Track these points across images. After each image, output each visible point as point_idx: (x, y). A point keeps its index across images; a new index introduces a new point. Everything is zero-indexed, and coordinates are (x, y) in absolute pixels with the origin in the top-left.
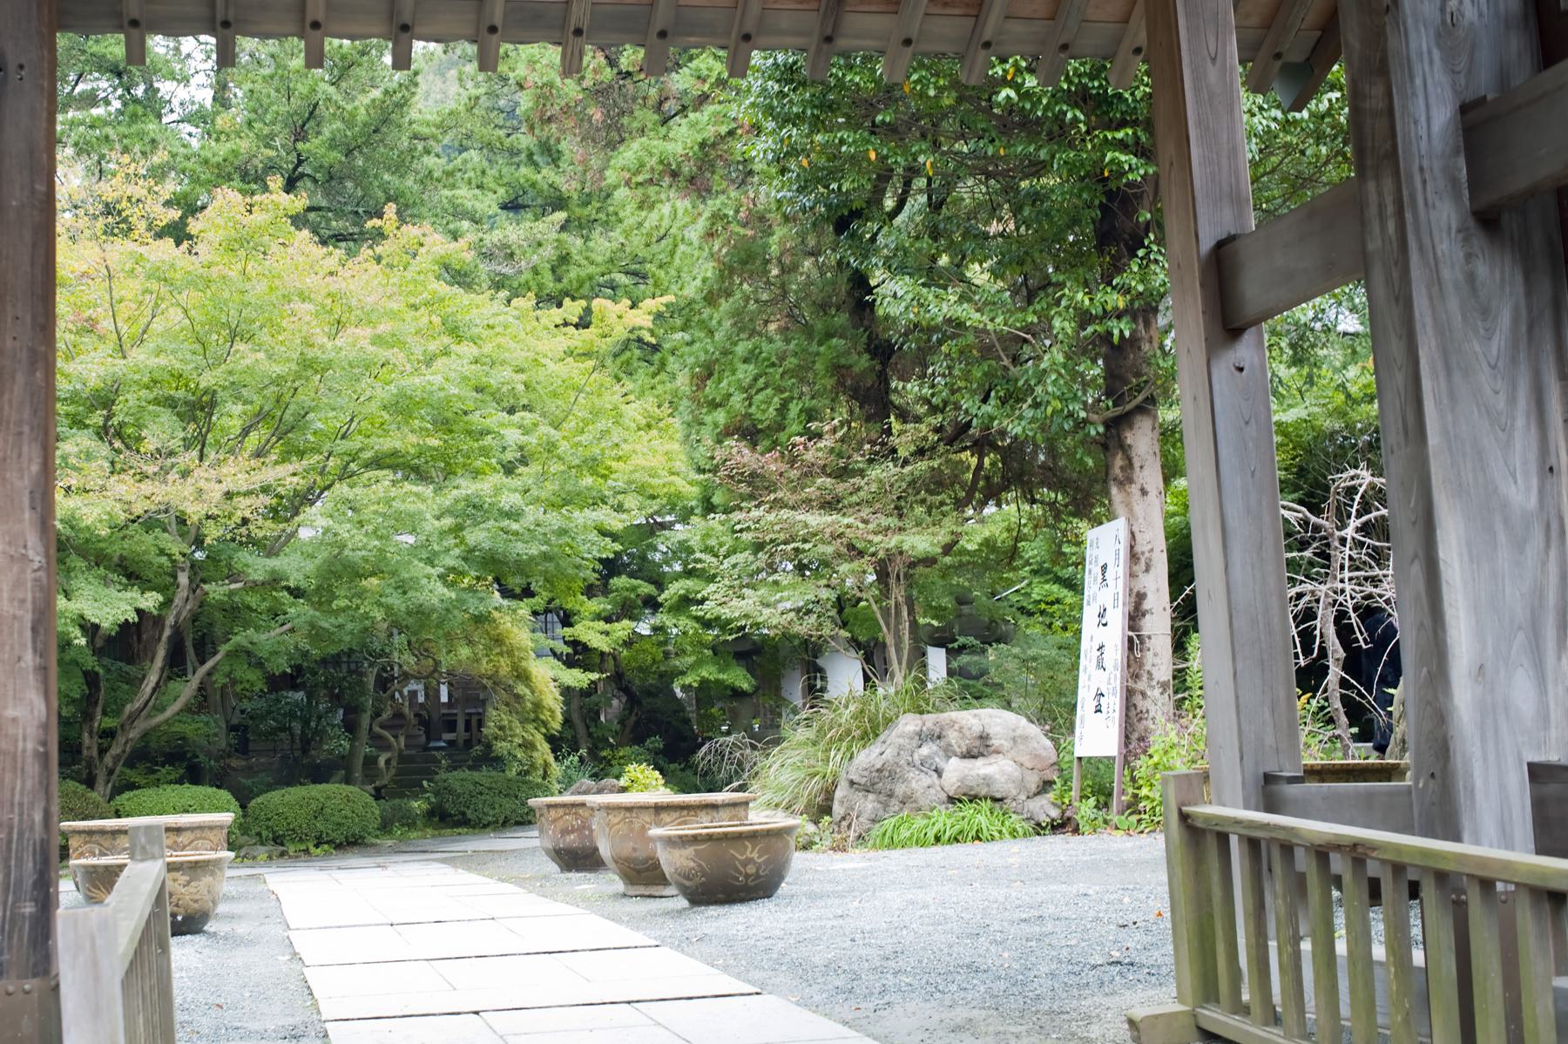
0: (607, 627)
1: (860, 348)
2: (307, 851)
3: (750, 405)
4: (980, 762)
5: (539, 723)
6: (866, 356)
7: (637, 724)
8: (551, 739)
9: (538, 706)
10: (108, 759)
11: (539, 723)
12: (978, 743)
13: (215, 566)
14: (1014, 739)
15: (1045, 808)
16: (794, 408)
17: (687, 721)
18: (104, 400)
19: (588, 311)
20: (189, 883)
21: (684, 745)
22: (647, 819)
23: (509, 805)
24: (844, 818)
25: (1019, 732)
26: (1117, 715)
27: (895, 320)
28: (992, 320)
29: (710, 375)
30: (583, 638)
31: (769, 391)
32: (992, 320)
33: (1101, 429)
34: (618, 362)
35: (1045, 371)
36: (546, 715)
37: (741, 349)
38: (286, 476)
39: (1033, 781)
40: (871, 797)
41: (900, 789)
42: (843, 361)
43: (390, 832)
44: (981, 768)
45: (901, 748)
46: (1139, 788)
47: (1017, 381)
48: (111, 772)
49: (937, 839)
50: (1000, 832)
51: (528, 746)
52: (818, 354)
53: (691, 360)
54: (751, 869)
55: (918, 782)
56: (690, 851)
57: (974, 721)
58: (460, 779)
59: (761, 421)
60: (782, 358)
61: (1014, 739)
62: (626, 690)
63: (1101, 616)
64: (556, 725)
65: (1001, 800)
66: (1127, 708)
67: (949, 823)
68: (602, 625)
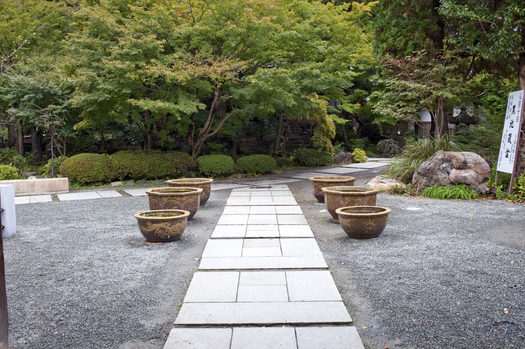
0: (352, 105)
1: (435, 23)
2: (253, 176)
3: (395, 42)
4: (463, 171)
5: (328, 136)
6: (436, 26)
7: (362, 132)
8: (331, 139)
9: (328, 130)
10: (195, 147)
11: (328, 136)
12: (462, 165)
13: (224, 89)
14: (476, 164)
15: (484, 187)
16: (410, 43)
17: (378, 130)
18: (188, 38)
19: (351, 6)
20: (171, 226)
21: (376, 137)
22: (340, 198)
23: (317, 160)
24: (415, 184)
25: (477, 161)
26: (514, 160)
27: (445, 16)
28: (481, 17)
29: (382, 31)
30: (345, 109)
31: (402, 37)
32: (481, 17)
33: (518, 57)
34: (362, 20)
35: (499, 36)
36: (330, 133)
37: (393, 22)
38: (243, 65)
39: (481, 178)
40: (425, 178)
41: (435, 177)
42: (428, 27)
43: (282, 167)
44: (464, 174)
45: (436, 163)
46: (519, 185)
47: (488, 39)
48: (196, 150)
49: (446, 197)
50: (468, 196)
51: (326, 143)
52: (420, 24)
53: (376, 26)
54: (370, 228)
55: (441, 176)
56: (349, 220)
57: (462, 157)
58: (303, 151)
59: (398, 47)
60: (407, 25)
61: (476, 164)
62: (359, 122)
63: (511, 123)
64: (333, 136)
65: (469, 184)
66: (518, 157)
67: (450, 191)
68: (351, 105)
